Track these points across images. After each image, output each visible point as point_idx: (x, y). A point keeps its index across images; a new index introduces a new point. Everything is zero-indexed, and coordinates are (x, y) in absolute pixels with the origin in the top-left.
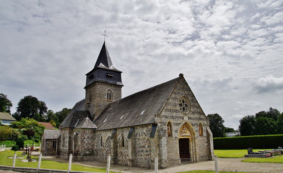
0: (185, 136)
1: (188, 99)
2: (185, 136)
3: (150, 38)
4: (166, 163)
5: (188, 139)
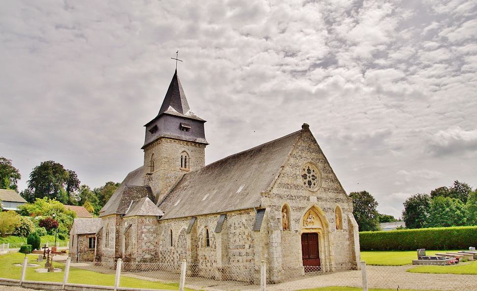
4: (280, 274)
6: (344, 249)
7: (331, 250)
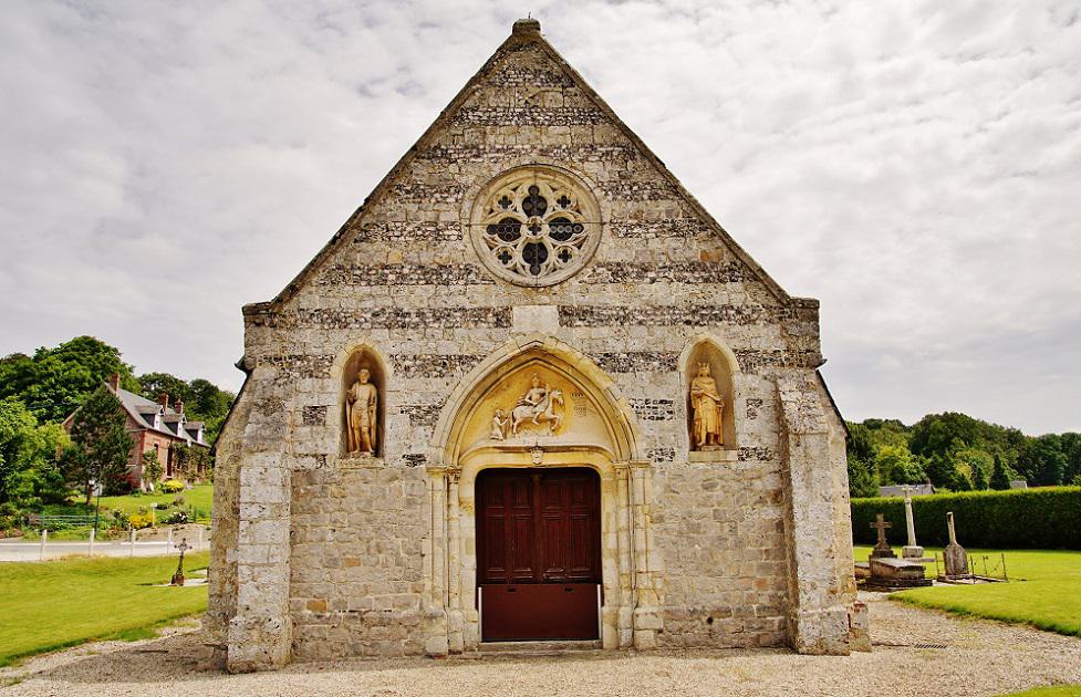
0: (545, 450)
1: (573, 182)
2: (545, 450)
3: (1006, 114)
4: (255, 634)
5: (587, 480)
6: (739, 544)
7: (641, 546)
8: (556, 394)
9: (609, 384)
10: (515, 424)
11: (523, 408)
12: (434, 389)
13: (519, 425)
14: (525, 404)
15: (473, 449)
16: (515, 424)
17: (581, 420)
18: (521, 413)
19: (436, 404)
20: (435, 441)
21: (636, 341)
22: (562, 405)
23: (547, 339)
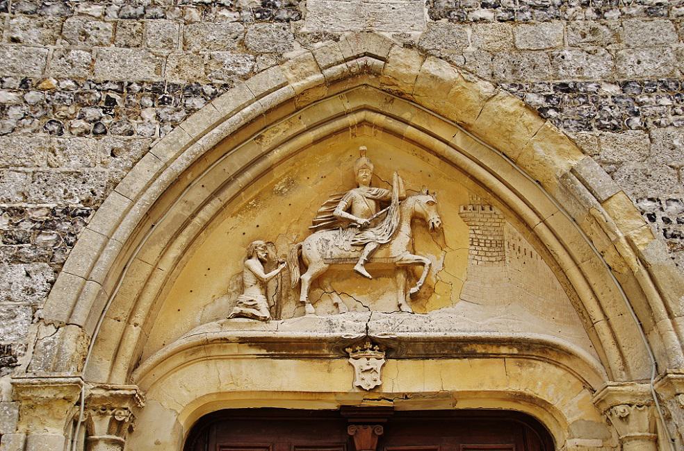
0: (393, 349)
2: (393, 349)
8: (418, 203)
9: (577, 160)
10: (307, 277)
11: (328, 235)
12: (75, 164)
13: (317, 282)
14: (334, 224)
15: (183, 342)
16: (307, 277)
17: (497, 270)
18: (323, 247)
19: (75, 203)
20: (53, 307)
21: (644, 55)
22: (436, 232)
23: (398, 51)
